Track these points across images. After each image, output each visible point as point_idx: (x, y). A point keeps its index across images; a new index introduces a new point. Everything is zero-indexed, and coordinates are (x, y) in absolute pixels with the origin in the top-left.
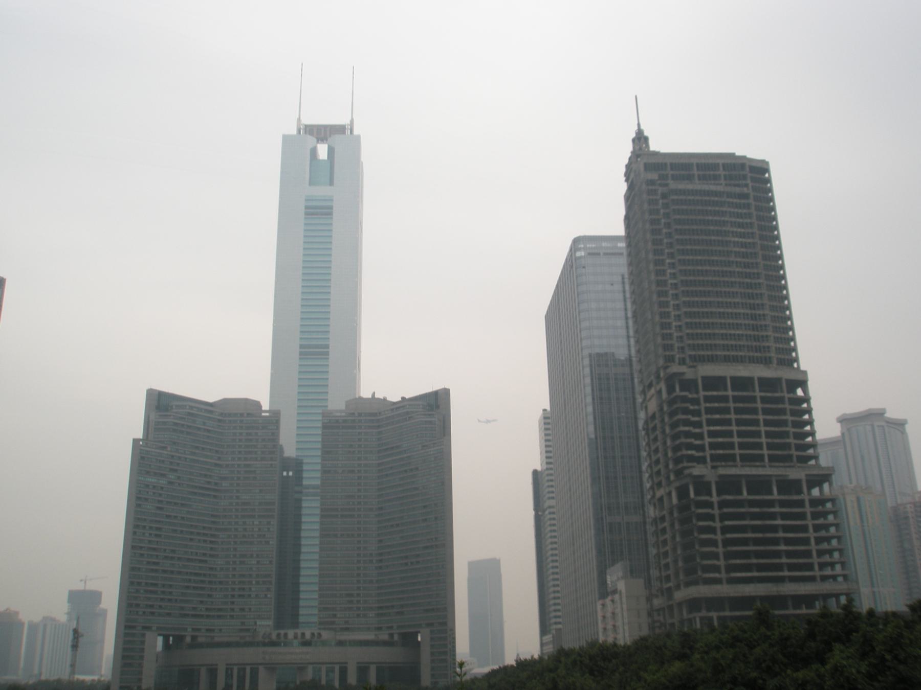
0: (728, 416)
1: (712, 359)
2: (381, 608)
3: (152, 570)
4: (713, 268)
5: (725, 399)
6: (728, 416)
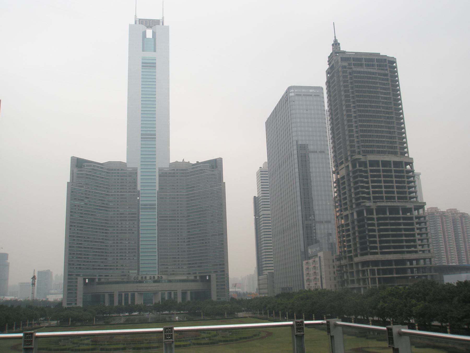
0: (380, 179)
1: (372, 152)
2: (190, 264)
3: (79, 247)
4: (373, 109)
5: (378, 171)
6: (380, 179)
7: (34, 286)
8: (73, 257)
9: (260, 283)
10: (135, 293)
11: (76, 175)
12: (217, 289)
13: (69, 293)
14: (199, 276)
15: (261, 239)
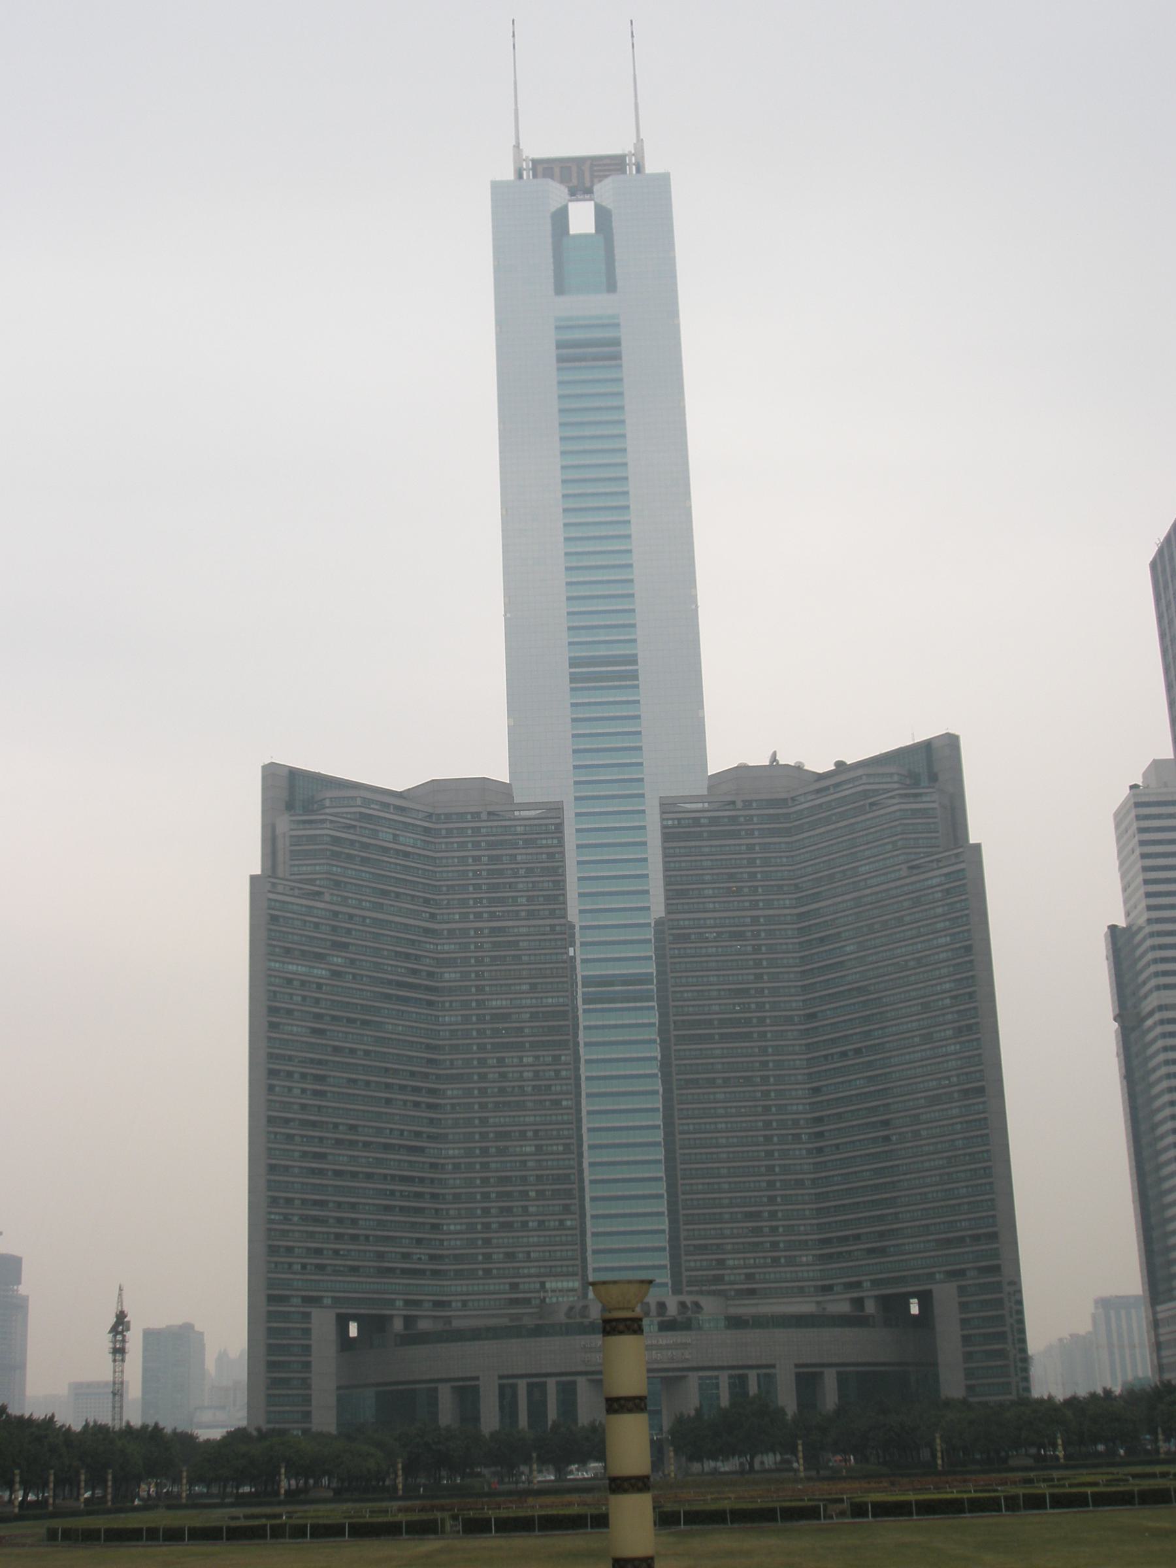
3: (313, 1172)
7: (123, 1360)
8: (287, 1219)
10: (574, 1383)
12: (968, 1357)
14: (877, 1297)
15: (1154, 1127)
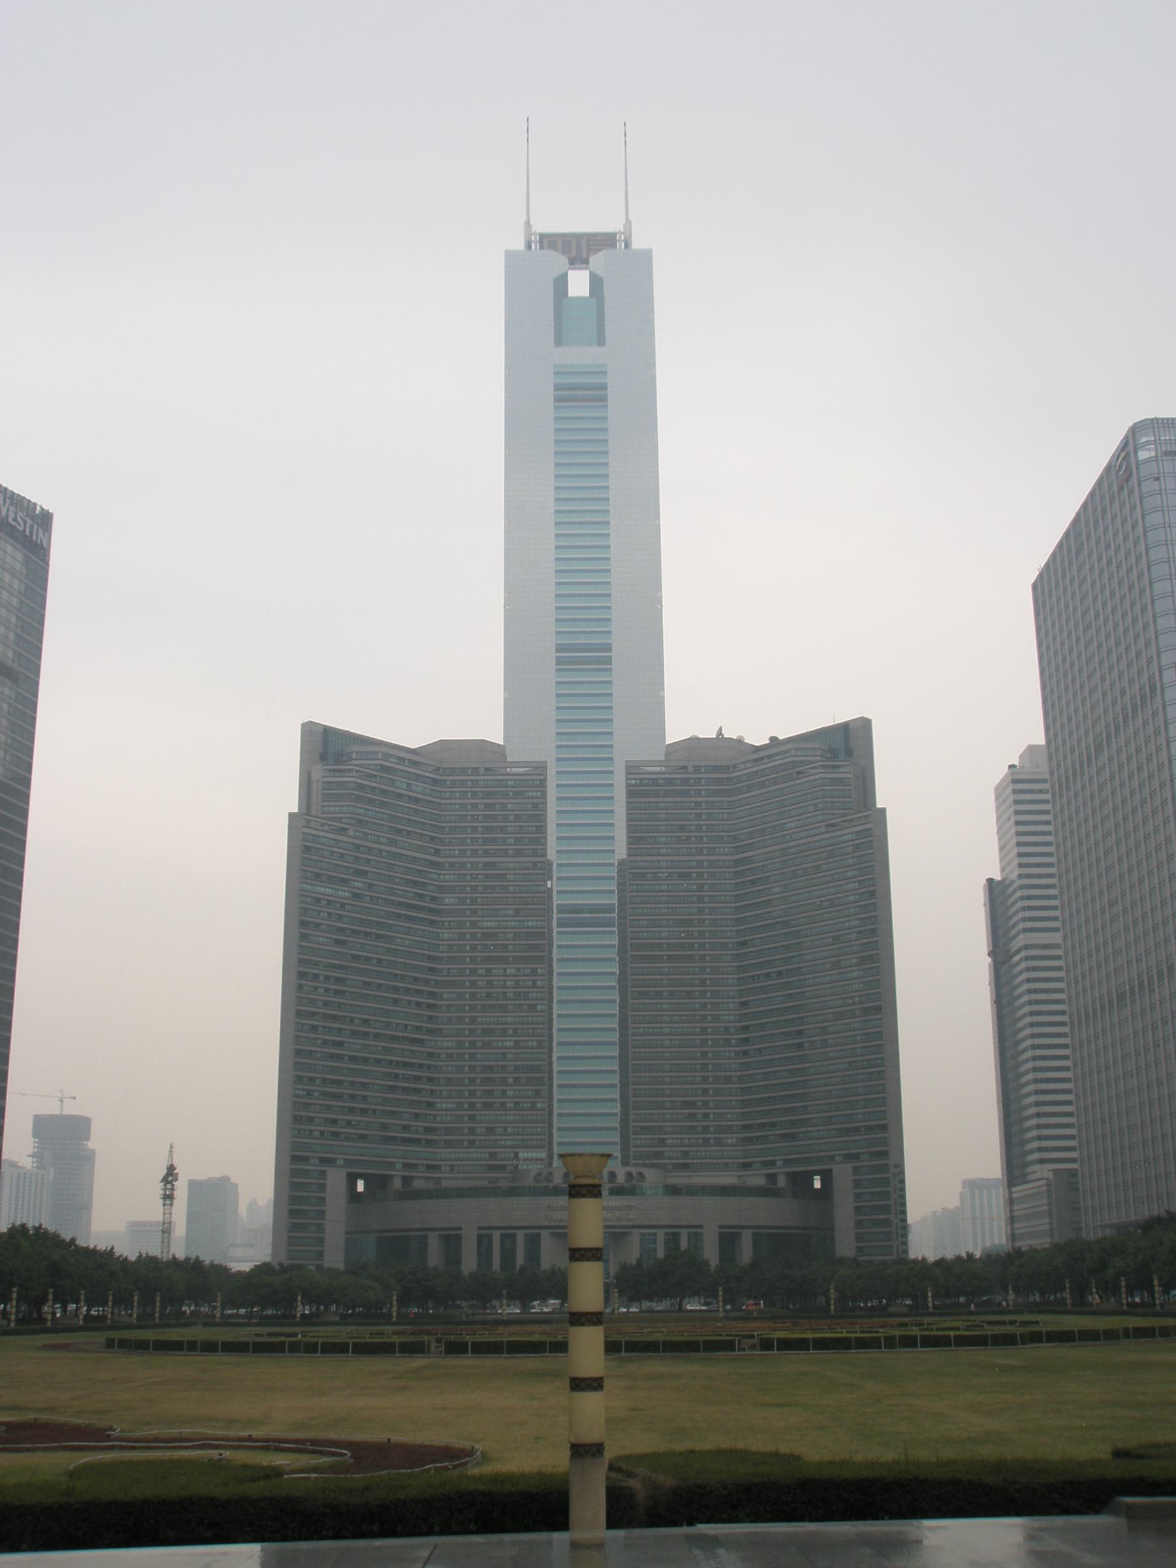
3: (332, 1056)
7: (171, 1205)
9: (1015, 1214)
10: (539, 1235)
11: (320, 788)
12: (859, 1224)
13: (294, 1227)
14: (787, 1174)
15: (1017, 1043)
